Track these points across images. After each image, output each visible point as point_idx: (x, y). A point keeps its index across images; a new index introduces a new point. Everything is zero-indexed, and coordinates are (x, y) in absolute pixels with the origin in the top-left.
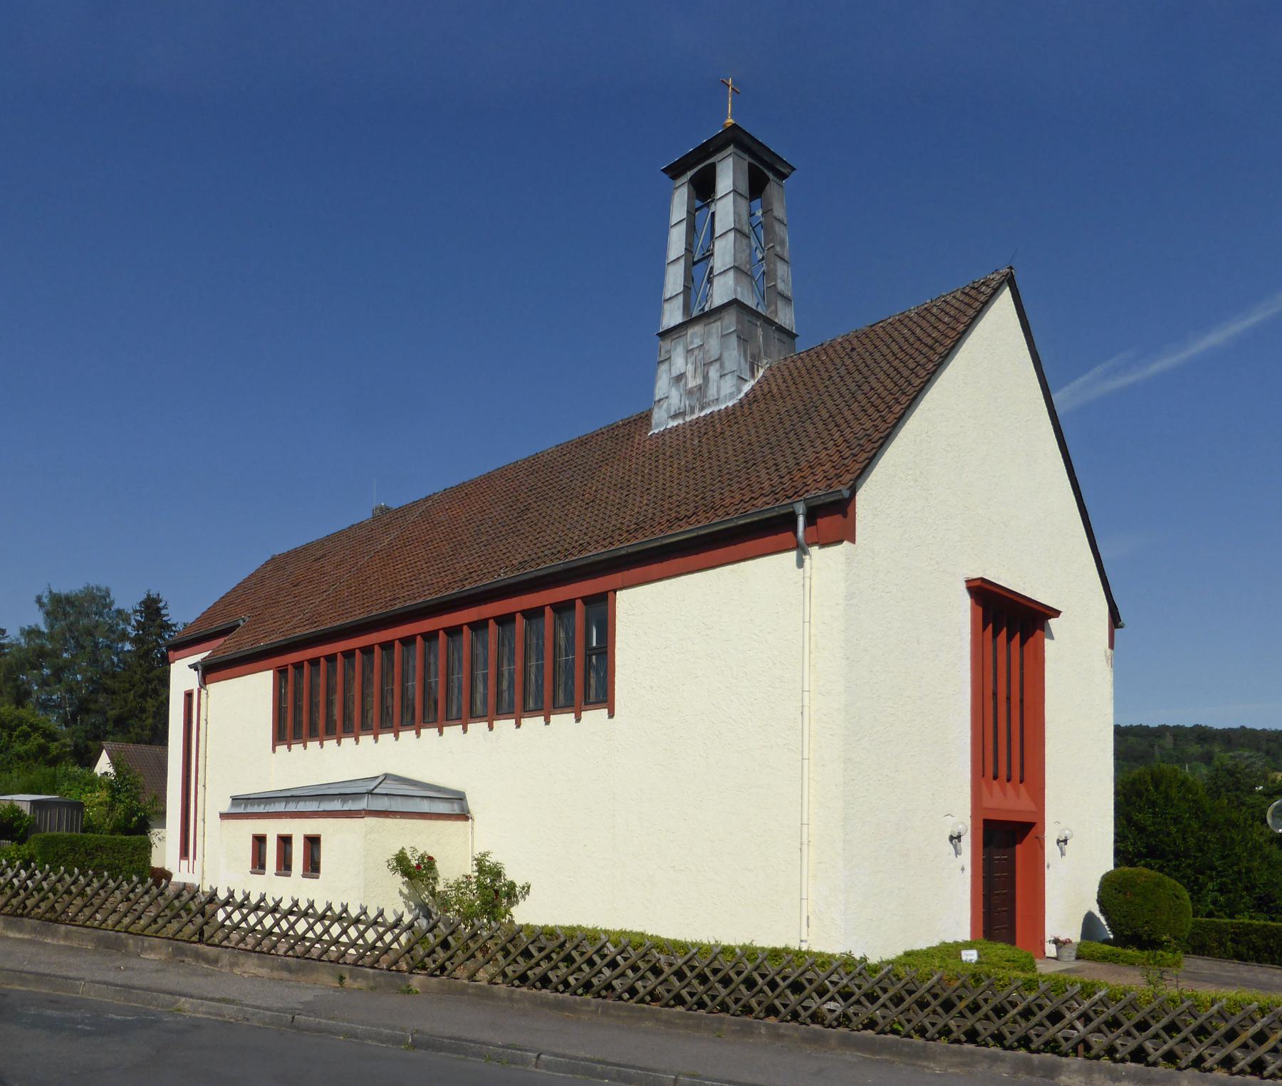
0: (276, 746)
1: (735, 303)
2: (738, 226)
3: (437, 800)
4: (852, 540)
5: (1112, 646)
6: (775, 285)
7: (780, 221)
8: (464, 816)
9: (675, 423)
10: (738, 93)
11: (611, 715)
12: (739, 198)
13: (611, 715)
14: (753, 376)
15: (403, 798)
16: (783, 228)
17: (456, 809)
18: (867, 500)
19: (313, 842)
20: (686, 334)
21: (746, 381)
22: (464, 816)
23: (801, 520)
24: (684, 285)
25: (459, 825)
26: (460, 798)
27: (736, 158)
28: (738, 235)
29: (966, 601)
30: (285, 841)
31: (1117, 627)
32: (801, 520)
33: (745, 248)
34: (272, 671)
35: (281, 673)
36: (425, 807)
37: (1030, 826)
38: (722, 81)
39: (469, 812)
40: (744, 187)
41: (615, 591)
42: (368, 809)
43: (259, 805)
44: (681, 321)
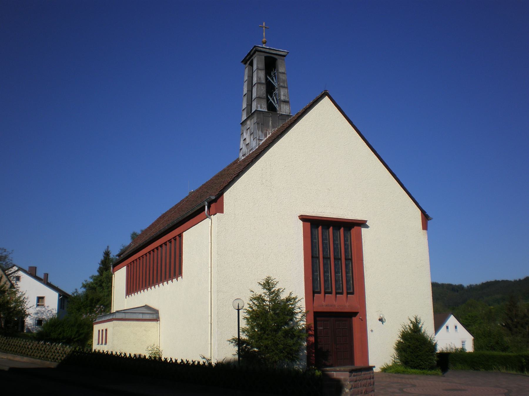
0: (60, 296)
1: (256, 110)
2: (258, 81)
3: (146, 314)
4: (222, 211)
5: (425, 227)
6: (280, 99)
7: (283, 73)
8: (157, 319)
9: (243, 158)
10: (268, 28)
11: (182, 278)
12: (259, 71)
13: (182, 278)
14: (266, 136)
15: (131, 313)
16: (284, 75)
17: (155, 317)
18: (227, 196)
19: (106, 330)
20: (246, 124)
21: (262, 140)
22: (157, 319)
23: (206, 207)
24: (247, 105)
25: (154, 323)
26: (156, 312)
27: (258, 56)
28: (259, 85)
29: (301, 223)
30: (102, 330)
31: (429, 220)
32: (206, 207)
33: (263, 89)
34: (125, 267)
35: (128, 266)
36: (140, 316)
37: (355, 314)
38: (260, 26)
39: (159, 318)
40: (262, 65)
41: (183, 232)
42: (116, 318)
43: (102, 318)
44: (246, 118)
